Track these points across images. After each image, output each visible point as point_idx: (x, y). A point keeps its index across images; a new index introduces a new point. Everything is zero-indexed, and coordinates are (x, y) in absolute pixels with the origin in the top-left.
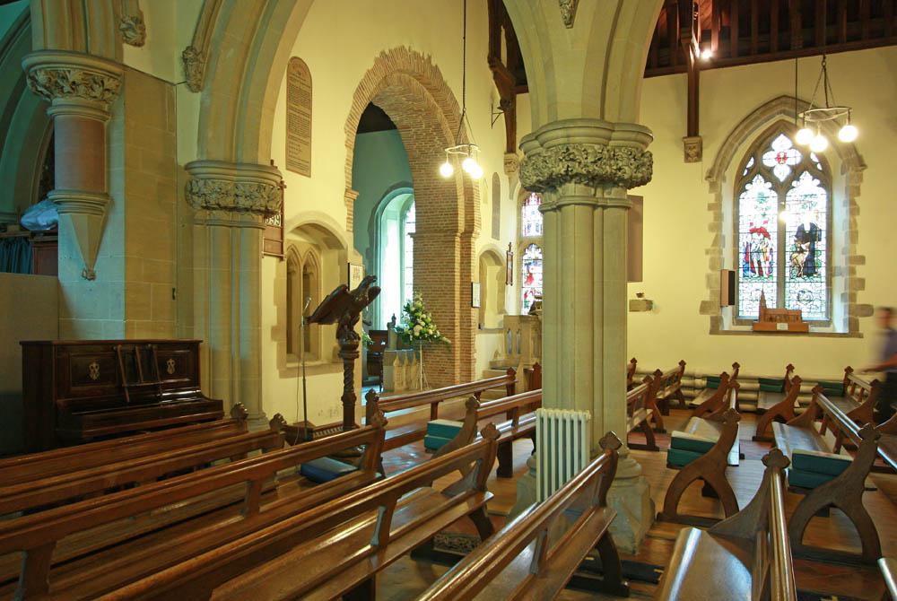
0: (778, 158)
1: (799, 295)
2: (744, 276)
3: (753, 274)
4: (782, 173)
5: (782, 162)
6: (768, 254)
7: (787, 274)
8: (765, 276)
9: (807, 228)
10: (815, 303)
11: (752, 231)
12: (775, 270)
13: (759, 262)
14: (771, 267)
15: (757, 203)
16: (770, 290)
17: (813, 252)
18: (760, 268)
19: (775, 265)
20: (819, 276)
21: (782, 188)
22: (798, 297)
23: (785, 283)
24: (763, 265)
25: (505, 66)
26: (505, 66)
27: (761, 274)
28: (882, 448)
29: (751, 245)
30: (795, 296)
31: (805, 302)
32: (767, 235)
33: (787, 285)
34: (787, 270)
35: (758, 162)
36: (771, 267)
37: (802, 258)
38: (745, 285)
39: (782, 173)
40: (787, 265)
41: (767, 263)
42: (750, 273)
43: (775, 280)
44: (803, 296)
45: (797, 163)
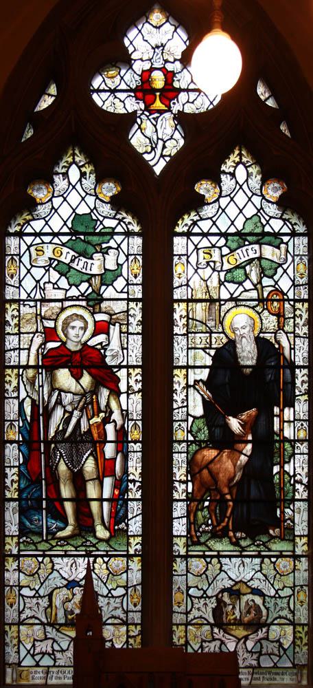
0: (144, 91)
1: (220, 602)
2: (23, 530)
3: (54, 524)
4: (157, 141)
5: (158, 105)
6: (109, 450)
7: (179, 527)
8: (102, 533)
9: (247, 353)
10: (275, 632)
11: (51, 362)
12: (135, 508)
13: (79, 481)
14: (119, 502)
15: (67, 255)
16: (119, 579)
17: (269, 446)
18: (81, 501)
19: (135, 493)
20: (288, 534)
21: (160, 204)
22: (218, 612)
23: (172, 558)
24: (92, 491)
25: (289, 135)
26: (289, 135)
27: (85, 524)
28: (280, 363)
29: (48, 414)
30: (206, 611)
31: (241, 632)
32: (106, 377)
33: (179, 566)
34: (179, 509)
35: (77, 95)
36: (119, 502)
37: (230, 465)
38: (29, 563)
39: (157, 141)
40: (180, 491)
41: (108, 482)
42: (45, 521)
43: (135, 545)
44: (236, 611)
45: (237, 350)
